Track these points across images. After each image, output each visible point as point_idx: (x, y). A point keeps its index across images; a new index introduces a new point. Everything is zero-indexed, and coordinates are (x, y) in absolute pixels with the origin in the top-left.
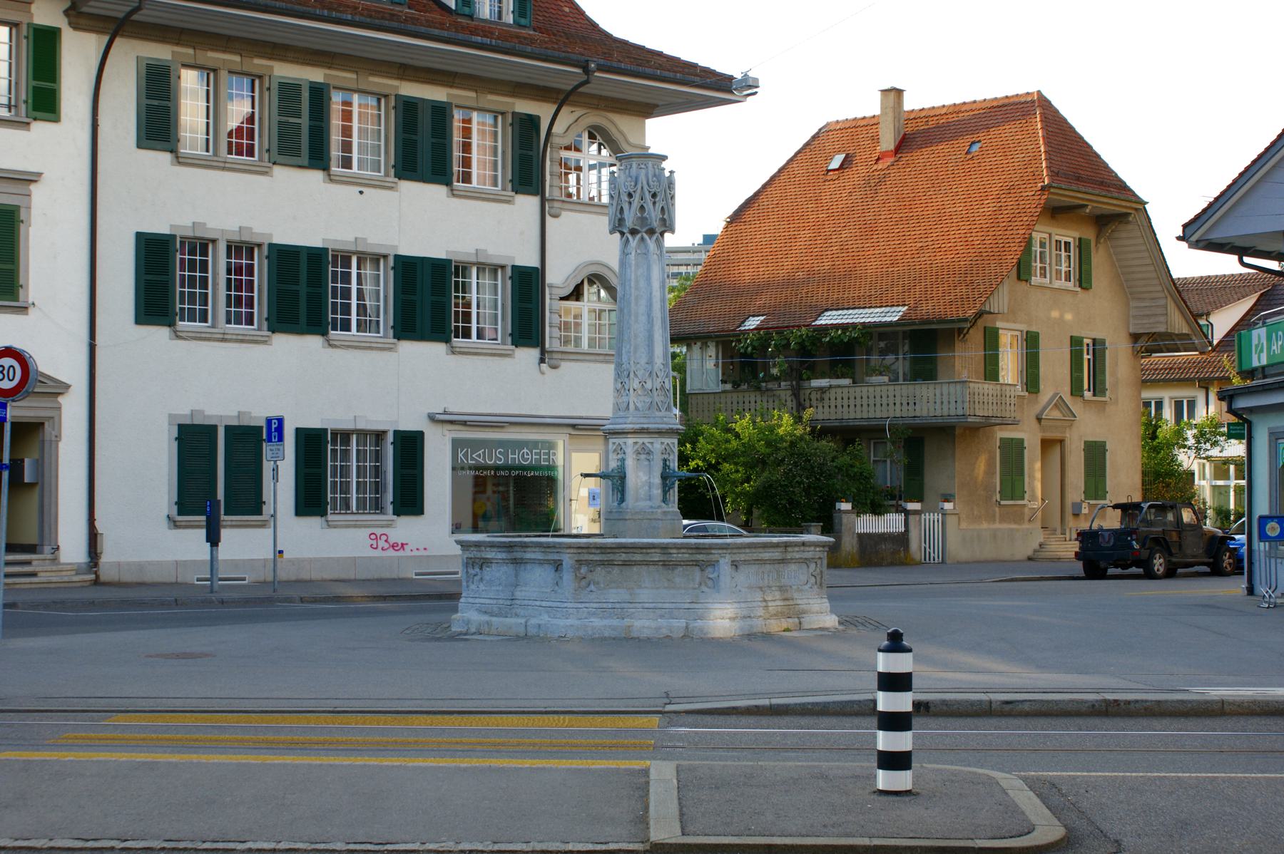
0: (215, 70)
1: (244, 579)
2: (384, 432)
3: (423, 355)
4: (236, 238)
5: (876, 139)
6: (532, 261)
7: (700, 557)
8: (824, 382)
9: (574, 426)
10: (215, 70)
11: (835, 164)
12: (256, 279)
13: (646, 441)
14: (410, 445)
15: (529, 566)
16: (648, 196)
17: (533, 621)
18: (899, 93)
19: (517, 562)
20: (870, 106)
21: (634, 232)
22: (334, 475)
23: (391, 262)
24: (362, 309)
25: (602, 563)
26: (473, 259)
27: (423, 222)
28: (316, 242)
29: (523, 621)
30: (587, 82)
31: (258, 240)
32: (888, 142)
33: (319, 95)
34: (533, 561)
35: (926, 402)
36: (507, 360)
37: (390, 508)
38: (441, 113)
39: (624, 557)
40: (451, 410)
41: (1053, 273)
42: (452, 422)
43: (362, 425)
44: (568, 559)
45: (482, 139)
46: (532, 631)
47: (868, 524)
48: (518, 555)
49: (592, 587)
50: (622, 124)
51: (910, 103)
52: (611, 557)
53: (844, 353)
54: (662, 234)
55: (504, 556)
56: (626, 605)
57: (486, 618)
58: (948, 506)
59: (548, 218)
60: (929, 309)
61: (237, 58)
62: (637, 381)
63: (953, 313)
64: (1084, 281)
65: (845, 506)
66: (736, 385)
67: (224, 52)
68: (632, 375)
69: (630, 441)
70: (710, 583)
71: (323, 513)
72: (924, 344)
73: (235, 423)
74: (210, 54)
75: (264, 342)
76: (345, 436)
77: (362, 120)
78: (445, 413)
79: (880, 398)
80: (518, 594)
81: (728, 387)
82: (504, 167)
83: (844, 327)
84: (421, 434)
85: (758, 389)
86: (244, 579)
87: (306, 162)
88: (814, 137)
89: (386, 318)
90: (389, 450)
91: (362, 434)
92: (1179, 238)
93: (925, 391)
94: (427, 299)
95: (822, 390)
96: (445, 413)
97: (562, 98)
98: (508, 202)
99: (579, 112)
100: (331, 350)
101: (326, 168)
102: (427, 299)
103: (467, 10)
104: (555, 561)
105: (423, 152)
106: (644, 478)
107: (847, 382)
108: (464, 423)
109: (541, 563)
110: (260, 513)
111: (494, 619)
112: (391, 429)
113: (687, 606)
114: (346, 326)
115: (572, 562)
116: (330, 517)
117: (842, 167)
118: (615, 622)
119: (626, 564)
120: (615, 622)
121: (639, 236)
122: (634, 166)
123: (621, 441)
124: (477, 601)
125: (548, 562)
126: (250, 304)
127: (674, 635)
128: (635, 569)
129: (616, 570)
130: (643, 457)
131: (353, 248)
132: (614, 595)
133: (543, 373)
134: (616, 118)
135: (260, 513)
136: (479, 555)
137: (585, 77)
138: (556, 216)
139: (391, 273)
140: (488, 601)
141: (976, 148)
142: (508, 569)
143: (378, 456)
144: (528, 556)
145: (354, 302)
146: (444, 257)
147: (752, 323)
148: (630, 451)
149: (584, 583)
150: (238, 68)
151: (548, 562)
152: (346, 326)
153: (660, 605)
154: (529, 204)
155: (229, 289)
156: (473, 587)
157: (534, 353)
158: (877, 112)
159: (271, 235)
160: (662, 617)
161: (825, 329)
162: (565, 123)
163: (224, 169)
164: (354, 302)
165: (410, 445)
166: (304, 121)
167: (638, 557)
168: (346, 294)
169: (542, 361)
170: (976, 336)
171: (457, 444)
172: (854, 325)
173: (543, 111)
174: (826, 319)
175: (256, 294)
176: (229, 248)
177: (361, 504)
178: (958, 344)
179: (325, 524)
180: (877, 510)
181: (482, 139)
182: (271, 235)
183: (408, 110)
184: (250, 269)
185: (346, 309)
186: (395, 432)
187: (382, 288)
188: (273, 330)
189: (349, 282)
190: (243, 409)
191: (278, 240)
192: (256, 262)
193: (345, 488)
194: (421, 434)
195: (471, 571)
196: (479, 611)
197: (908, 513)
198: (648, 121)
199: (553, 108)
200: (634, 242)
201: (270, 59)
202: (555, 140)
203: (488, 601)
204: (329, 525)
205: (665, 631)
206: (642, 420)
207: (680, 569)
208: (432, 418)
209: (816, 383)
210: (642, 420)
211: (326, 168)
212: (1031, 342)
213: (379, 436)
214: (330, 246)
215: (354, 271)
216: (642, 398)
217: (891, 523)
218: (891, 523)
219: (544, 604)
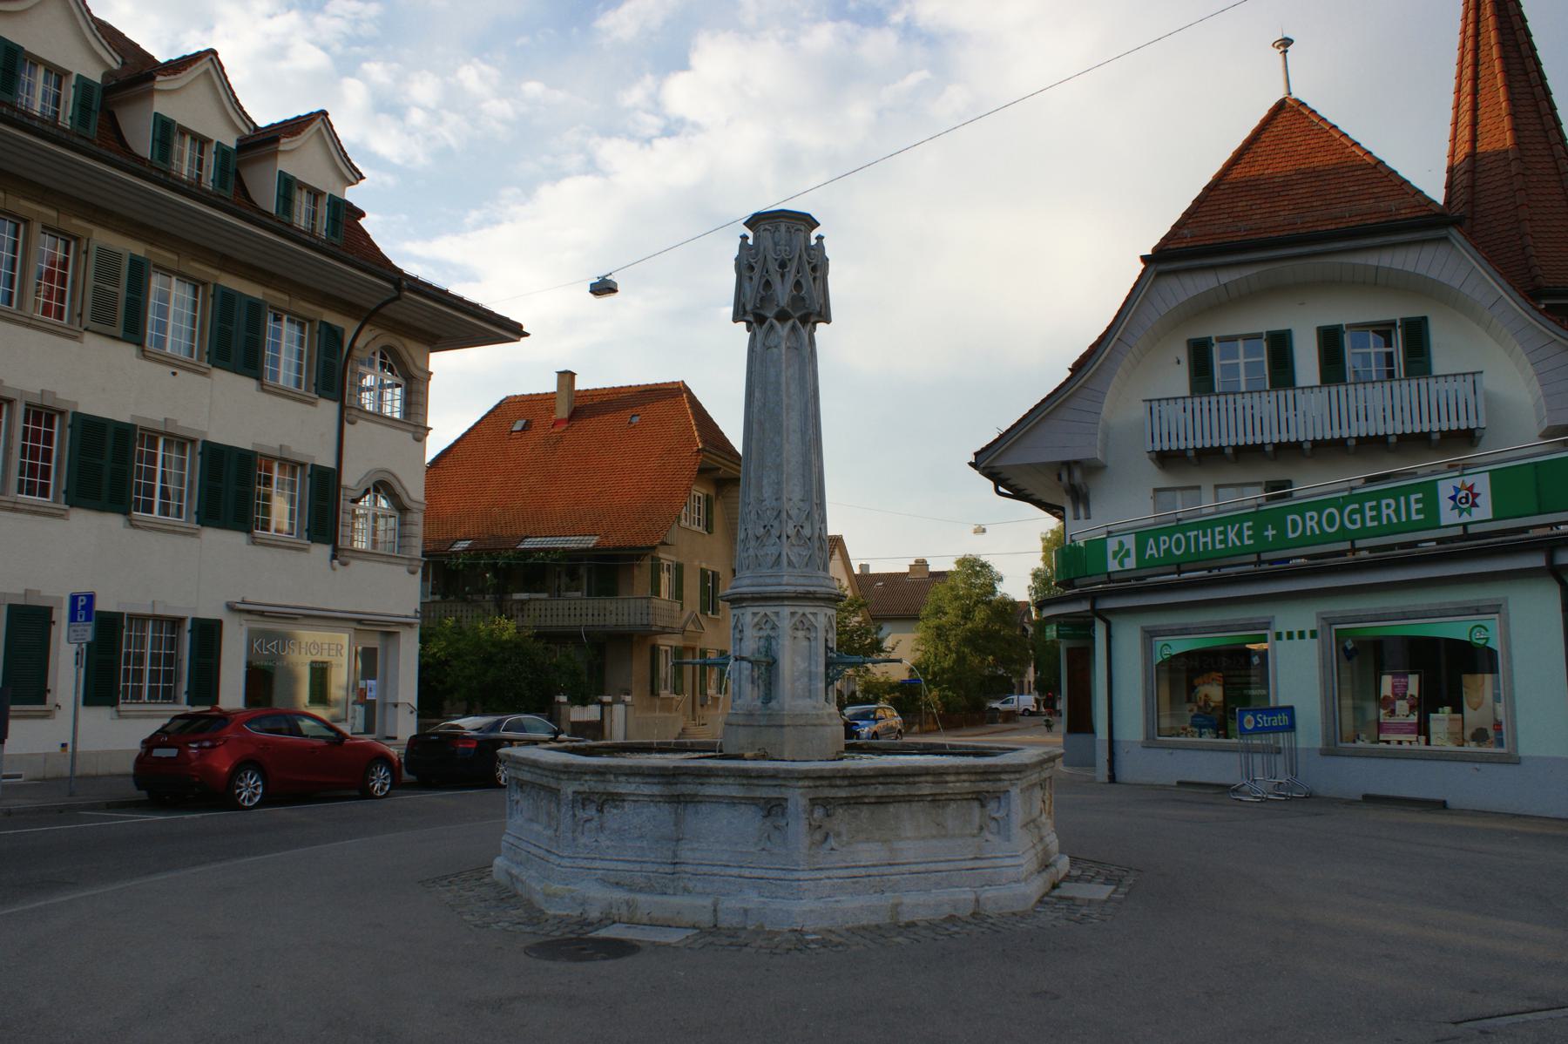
0: (26, 221)
1: (19, 776)
2: (181, 620)
3: (224, 543)
4: (37, 401)
5: (552, 410)
6: (329, 462)
7: (984, 786)
8: (524, 596)
9: (360, 621)
10: (26, 221)
11: (518, 426)
12: (55, 448)
13: (808, 610)
14: (208, 634)
15: (704, 808)
16: (808, 268)
17: (730, 903)
18: (573, 375)
19: (677, 800)
20: (549, 385)
21: (782, 316)
22: (127, 663)
23: (199, 447)
24: (165, 493)
25: (848, 802)
26: (277, 454)
27: (230, 411)
28: (124, 417)
29: (708, 902)
30: (398, 298)
31: (63, 407)
32: (562, 412)
33: (139, 273)
34: (717, 800)
35: (616, 612)
36: (304, 554)
37: (184, 698)
38: (255, 310)
39: (881, 790)
40: (249, 599)
41: (690, 519)
42: (249, 612)
43: (159, 611)
44: (797, 798)
45: (286, 347)
46: (726, 921)
47: (578, 714)
48: (688, 789)
49: (832, 842)
50: (411, 349)
51: (581, 384)
52: (861, 791)
53: (536, 572)
54: (814, 324)
55: (656, 790)
56: (886, 870)
57: (619, 895)
58: (628, 698)
59: (347, 425)
60: (615, 540)
61: (54, 214)
62: (791, 524)
63: (640, 543)
64: (709, 527)
65: (563, 699)
66: (445, 597)
67: (39, 203)
68: (784, 515)
69: (786, 611)
70: (993, 825)
71: (113, 703)
72: (607, 569)
73: (21, 602)
74: (23, 203)
75: (60, 516)
76: (140, 620)
77: (174, 305)
78: (243, 602)
79: (577, 609)
80: (686, 854)
81: (438, 597)
82: (308, 371)
83: (547, 551)
84: (220, 622)
85: (465, 600)
86: (19, 776)
87: (119, 331)
88: (497, 407)
89: (190, 504)
90: (187, 637)
91: (158, 620)
92: (971, 464)
93: (610, 604)
94: (229, 488)
95: (522, 602)
96: (243, 602)
97: (367, 316)
98: (312, 404)
99: (378, 331)
100: (132, 531)
101: (140, 344)
102: (229, 488)
103: (286, 219)
104: (768, 800)
105: (234, 345)
106: (803, 665)
107: (544, 596)
108: (261, 614)
109: (733, 802)
110: (44, 702)
111: (641, 898)
112: (190, 615)
113: (970, 864)
114: (148, 508)
115: (804, 802)
116: (122, 707)
117: (523, 429)
118: (874, 900)
119: (881, 801)
120: (874, 900)
121: (790, 322)
122: (783, 228)
123: (769, 610)
124: (597, 864)
125: (753, 801)
126: (46, 473)
127: (959, 913)
128: (891, 808)
129: (865, 812)
130: (800, 634)
131: (162, 428)
132: (868, 853)
133: (334, 569)
134: (407, 342)
135: (44, 702)
136: (600, 788)
137: (395, 294)
138: (352, 423)
139: (198, 458)
140: (621, 866)
141: (636, 419)
142: (665, 812)
143: (173, 643)
144: (709, 791)
145: (158, 484)
146: (249, 447)
147: (461, 545)
148: (786, 624)
149: (818, 836)
150: (53, 224)
151: (753, 801)
152: (148, 508)
153: (933, 867)
154: (329, 409)
155: (23, 456)
156: (582, 840)
157: (326, 550)
158: (554, 389)
159: (76, 404)
160: (937, 885)
161: (529, 553)
162: (368, 339)
163: (28, 326)
164: (158, 484)
165: (208, 634)
166: (122, 291)
167: (901, 790)
168: (151, 475)
169: (334, 557)
170: (647, 562)
171: (253, 636)
172: (556, 550)
173: (349, 326)
174: (527, 544)
175: (53, 465)
176: (27, 412)
177: (153, 693)
178: (636, 572)
179: (115, 715)
180: (584, 702)
181: (286, 347)
182: (76, 404)
183: (227, 300)
184: (49, 438)
185: (150, 491)
186: (194, 620)
187: (186, 473)
188: (72, 504)
189: (155, 463)
190: (31, 587)
191: (82, 409)
192: (56, 431)
193: (138, 675)
194: (220, 622)
195: (580, 814)
196: (603, 881)
197: (603, 704)
198: (432, 355)
199: (357, 325)
200: (783, 330)
201: (90, 222)
202: (356, 353)
203: (621, 866)
204: (120, 716)
205: (947, 910)
206: (802, 581)
207: (953, 805)
208: (231, 608)
209: (517, 596)
210: (802, 581)
211: (140, 344)
212: (679, 569)
213: (176, 623)
214: (140, 424)
215: (160, 452)
216: (796, 549)
217: (591, 713)
218: (591, 713)
219: (747, 872)
